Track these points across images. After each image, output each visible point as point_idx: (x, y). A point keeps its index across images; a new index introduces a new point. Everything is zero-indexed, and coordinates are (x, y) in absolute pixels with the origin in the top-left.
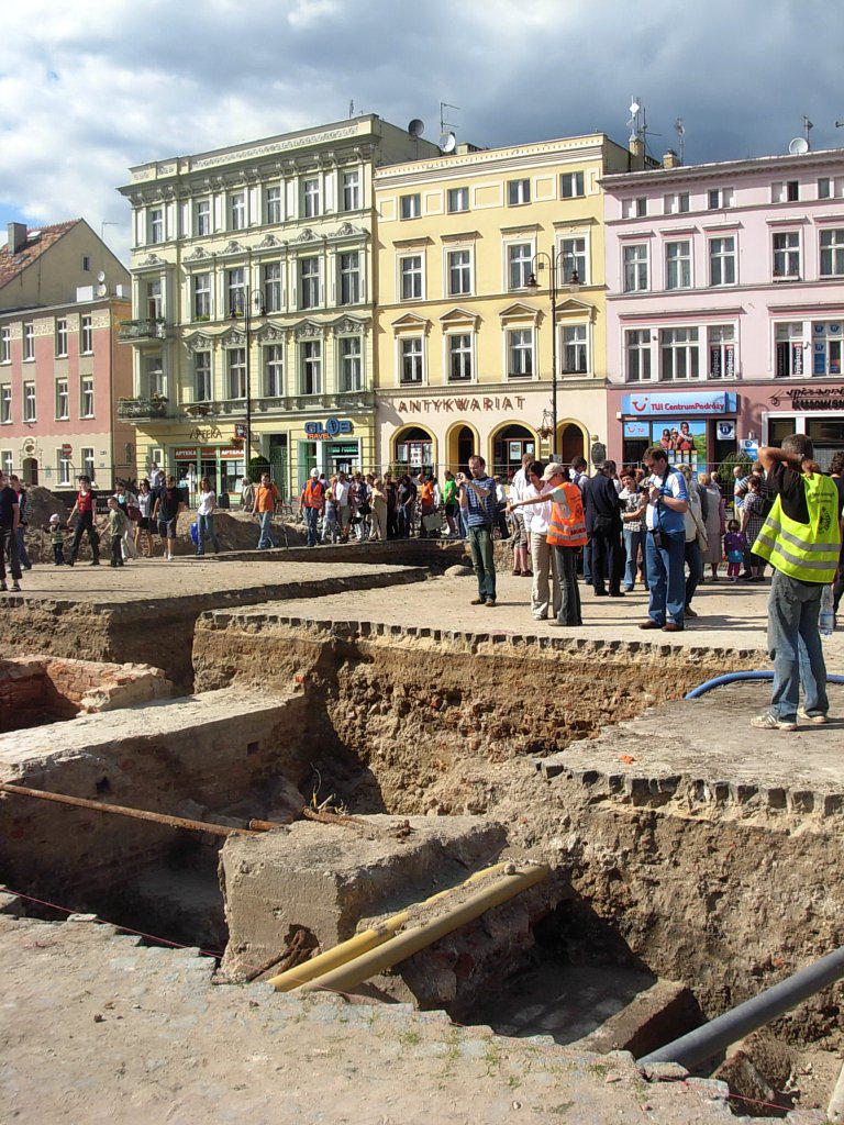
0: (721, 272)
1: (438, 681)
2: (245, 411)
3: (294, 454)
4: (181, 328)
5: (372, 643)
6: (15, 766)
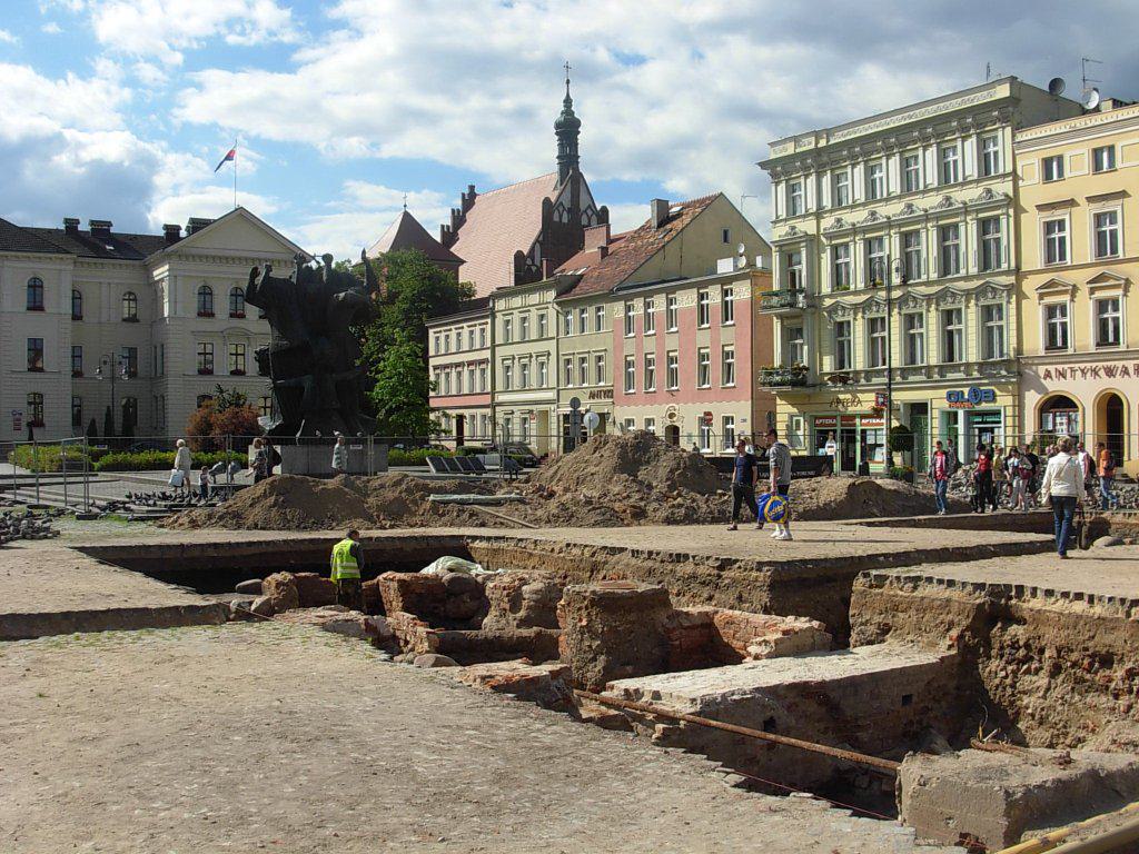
1: (1091, 644)
2: (886, 380)
3: (935, 426)
4: (822, 298)
5: (1025, 605)
6: (693, 700)
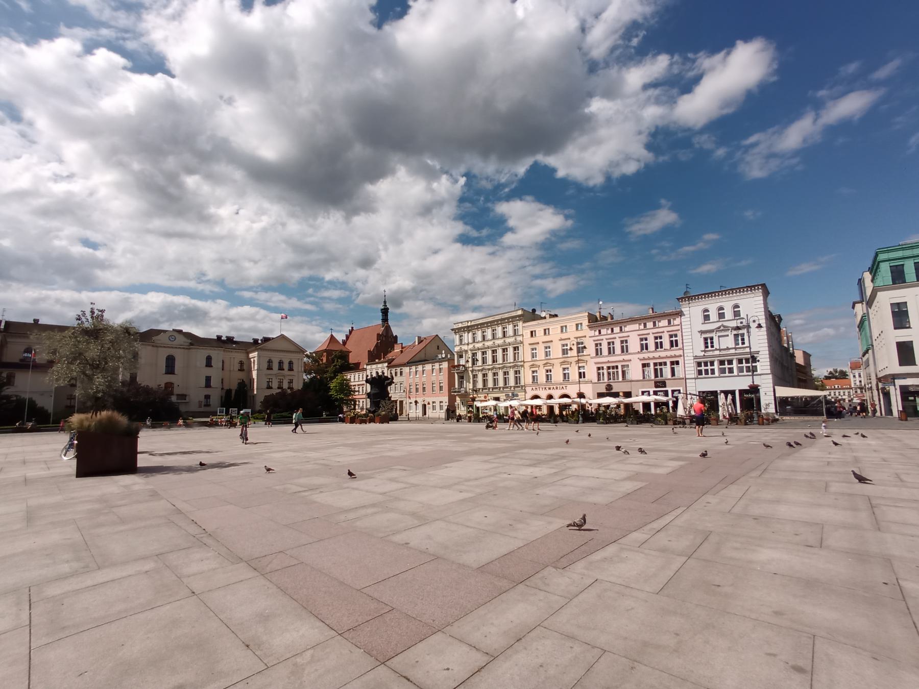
0: (625, 350)
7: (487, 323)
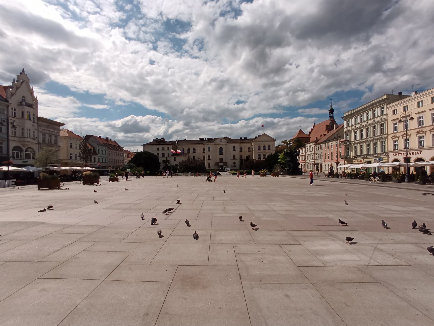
7: (362, 109)
